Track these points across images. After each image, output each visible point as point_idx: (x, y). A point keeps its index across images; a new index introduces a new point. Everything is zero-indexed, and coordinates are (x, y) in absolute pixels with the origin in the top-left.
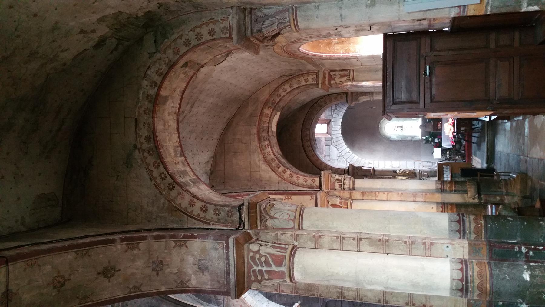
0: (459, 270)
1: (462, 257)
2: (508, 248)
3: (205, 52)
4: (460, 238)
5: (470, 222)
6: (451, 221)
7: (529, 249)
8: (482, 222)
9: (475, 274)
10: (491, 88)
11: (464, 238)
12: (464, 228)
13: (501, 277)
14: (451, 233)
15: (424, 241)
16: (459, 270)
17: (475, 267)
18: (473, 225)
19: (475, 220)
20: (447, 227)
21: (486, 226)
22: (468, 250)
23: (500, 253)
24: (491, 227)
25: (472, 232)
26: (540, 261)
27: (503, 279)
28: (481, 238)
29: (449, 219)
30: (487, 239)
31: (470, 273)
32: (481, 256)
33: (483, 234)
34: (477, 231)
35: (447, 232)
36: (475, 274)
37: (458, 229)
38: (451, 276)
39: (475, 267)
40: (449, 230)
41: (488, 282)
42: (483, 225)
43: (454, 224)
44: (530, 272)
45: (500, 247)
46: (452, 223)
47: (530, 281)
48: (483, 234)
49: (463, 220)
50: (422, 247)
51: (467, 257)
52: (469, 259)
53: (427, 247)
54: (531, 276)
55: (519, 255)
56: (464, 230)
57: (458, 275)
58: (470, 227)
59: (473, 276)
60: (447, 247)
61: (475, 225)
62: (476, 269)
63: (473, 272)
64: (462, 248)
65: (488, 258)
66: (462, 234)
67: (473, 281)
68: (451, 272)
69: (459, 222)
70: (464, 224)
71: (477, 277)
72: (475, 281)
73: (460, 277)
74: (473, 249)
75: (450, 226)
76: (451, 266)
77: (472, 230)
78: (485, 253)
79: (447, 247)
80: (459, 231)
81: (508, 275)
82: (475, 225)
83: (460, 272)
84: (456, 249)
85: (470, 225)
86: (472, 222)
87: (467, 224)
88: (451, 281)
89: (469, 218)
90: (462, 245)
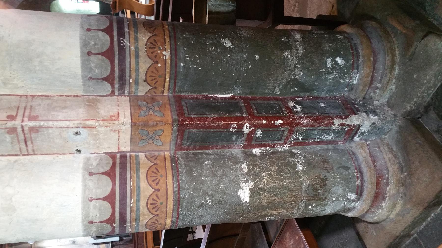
0: (105, 199)
1: (115, 150)
2: (217, 127)
3: (435, 23)
4: (112, 94)
5: (137, 56)
6: (89, 53)
7: (257, 127)
8: (167, 54)
9: (143, 203)
10: (117, 66)
11: (122, 94)
12: (122, 71)
13: (197, 203)
14: (91, 83)
15: (10, 124)
16: (105, 199)
17: (144, 184)
18: (145, 64)
19: (152, 46)
20: (79, 71)
21: (174, 65)
22: (129, 136)
23: (201, 123)
24: (186, 68)
25: (141, 81)
26: (270, 143)
27: (201, 205)
28: (163, 92)
29: (84, 44)
30: (174, 92)
31: (130, 202)
32: (160, 144)
33: (167, 84)
34: (153, 78)
35: (79, 82)
36: (143, 203)
37: (107, 73)
38: (85, 216)
39: (144, 184)
40: (83, 77)
41: (170, 214)
42: (169, 62)
43: (96, 60)
44: (251, 183)
45: (201, 127)
46: (92, 58)
47: (249, 203)
48: (167, 84)
49: (122, 49)
50: (8, 138)
51: (126, 147)
52: (131, 151)
53: (22, 137)
54: (254, 192)
55: (234, 137)
56: (122, 77)
57: (101, 211)
58: (137, 70)
59: (138, 209)
60: (77, 133)
61: (151, 62)
62: (147, 190)
63: (138, 200)
64: (116, 135)
65: (173, 147)
66: (117, 86)
67: (137, 219)
68: (85, 208)
69: (108, 54)
70: (122, 61)
71: (146, 211)
72: (141, 218)
73: (108, 215)
74: (141, 129)
75: (85, 65)
76: (85, 187)
77: (142, 76)
78: (168, 139)
79: (77, 133)
80: (109, 79)
81: (212, 197)
82: (151, 62)
83: (107, 205)
84: (101, 136)
85: (137, 63)
86: (143, 53)
87: (130, 61)
88: (84, 226)
89: (137, 40)
90: (117, 128)
